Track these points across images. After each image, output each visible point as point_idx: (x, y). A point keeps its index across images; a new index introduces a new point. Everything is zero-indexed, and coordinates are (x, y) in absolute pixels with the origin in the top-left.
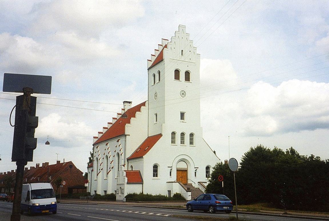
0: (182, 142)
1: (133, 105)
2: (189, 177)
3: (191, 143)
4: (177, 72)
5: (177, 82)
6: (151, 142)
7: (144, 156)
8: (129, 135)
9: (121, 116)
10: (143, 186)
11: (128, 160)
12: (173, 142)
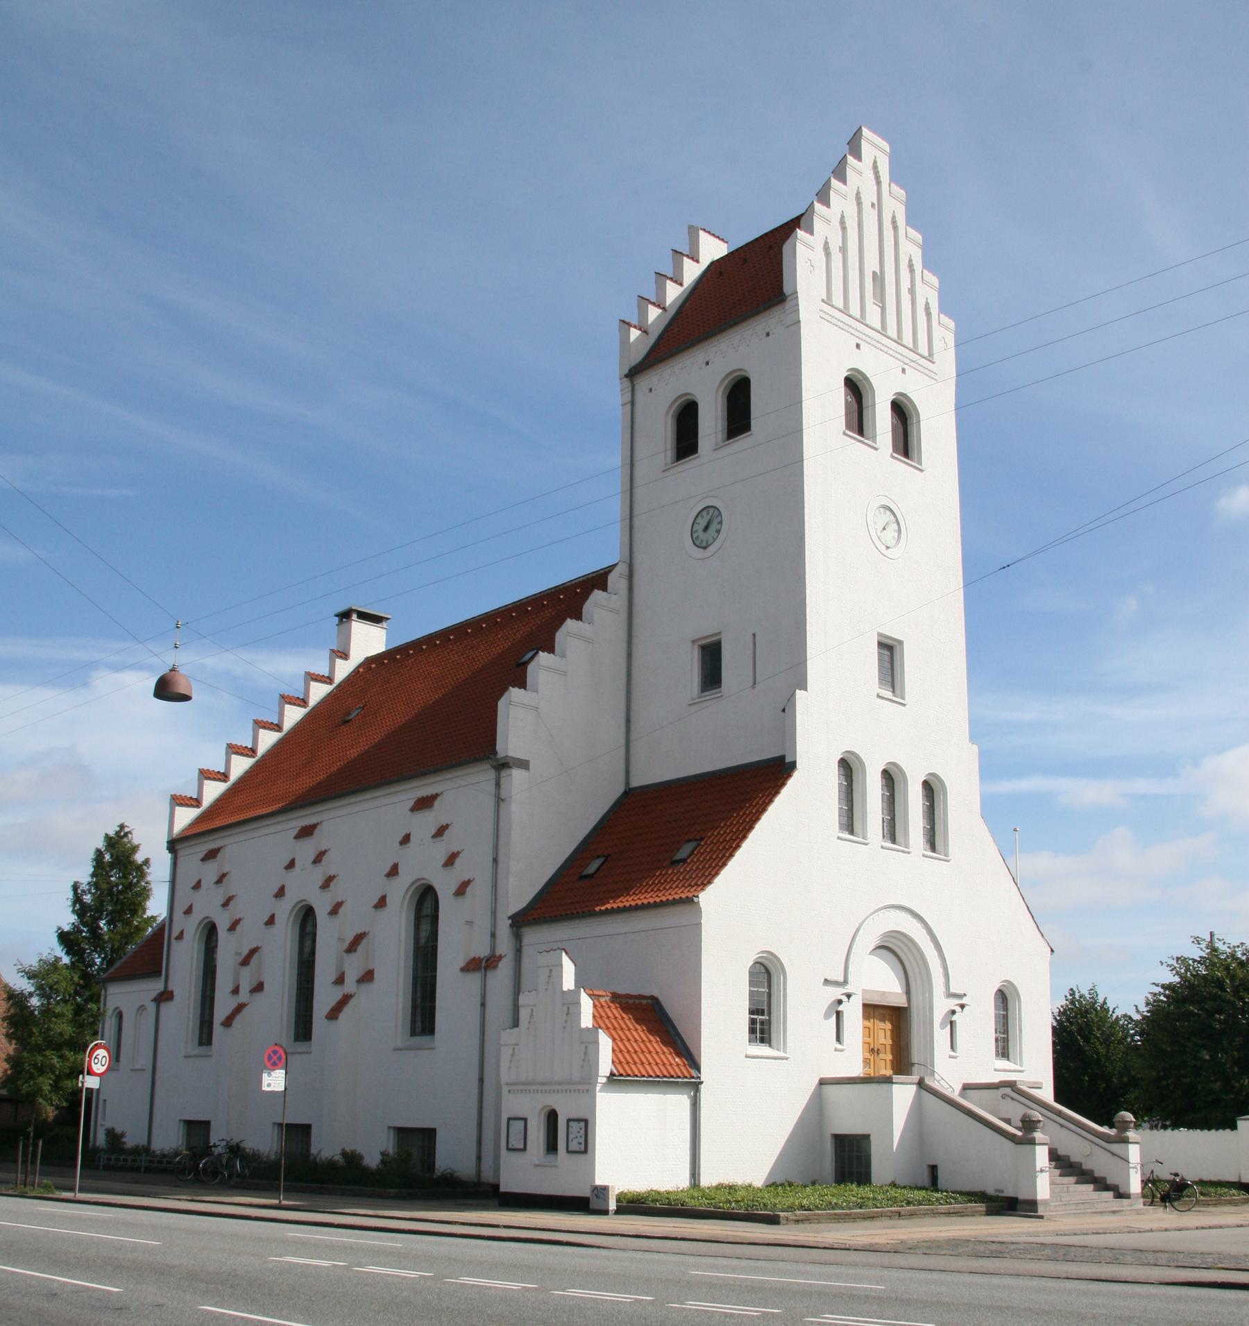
8: (524, 764)
12: (850, 822)
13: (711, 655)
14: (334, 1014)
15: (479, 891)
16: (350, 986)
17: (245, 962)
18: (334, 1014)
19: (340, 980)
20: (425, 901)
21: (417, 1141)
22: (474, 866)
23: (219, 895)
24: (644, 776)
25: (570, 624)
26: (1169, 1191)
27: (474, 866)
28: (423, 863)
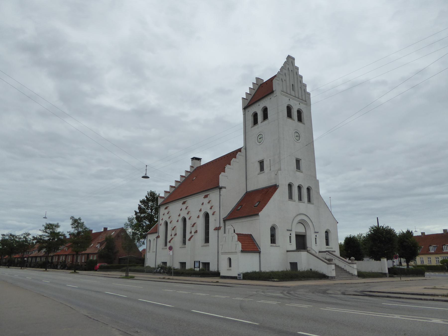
1: (203, 162)
7: (260, 213)
8: (225, 188)
10: (260, 256)
12: (291, 197)
13: (261, 163)
14: (189, 240)
15: (217, 213)
16: (193, 234)
17: (173, 229)
18: (189, 240)
19: (191, 233)
20: (207, 216)
21: (207, 265)
22: (216, 209)
23: (209, 206)
24: (251, 188)
25: (233, 159)
26: (361, 275)
27: (216, 209)
28: (206, 208)
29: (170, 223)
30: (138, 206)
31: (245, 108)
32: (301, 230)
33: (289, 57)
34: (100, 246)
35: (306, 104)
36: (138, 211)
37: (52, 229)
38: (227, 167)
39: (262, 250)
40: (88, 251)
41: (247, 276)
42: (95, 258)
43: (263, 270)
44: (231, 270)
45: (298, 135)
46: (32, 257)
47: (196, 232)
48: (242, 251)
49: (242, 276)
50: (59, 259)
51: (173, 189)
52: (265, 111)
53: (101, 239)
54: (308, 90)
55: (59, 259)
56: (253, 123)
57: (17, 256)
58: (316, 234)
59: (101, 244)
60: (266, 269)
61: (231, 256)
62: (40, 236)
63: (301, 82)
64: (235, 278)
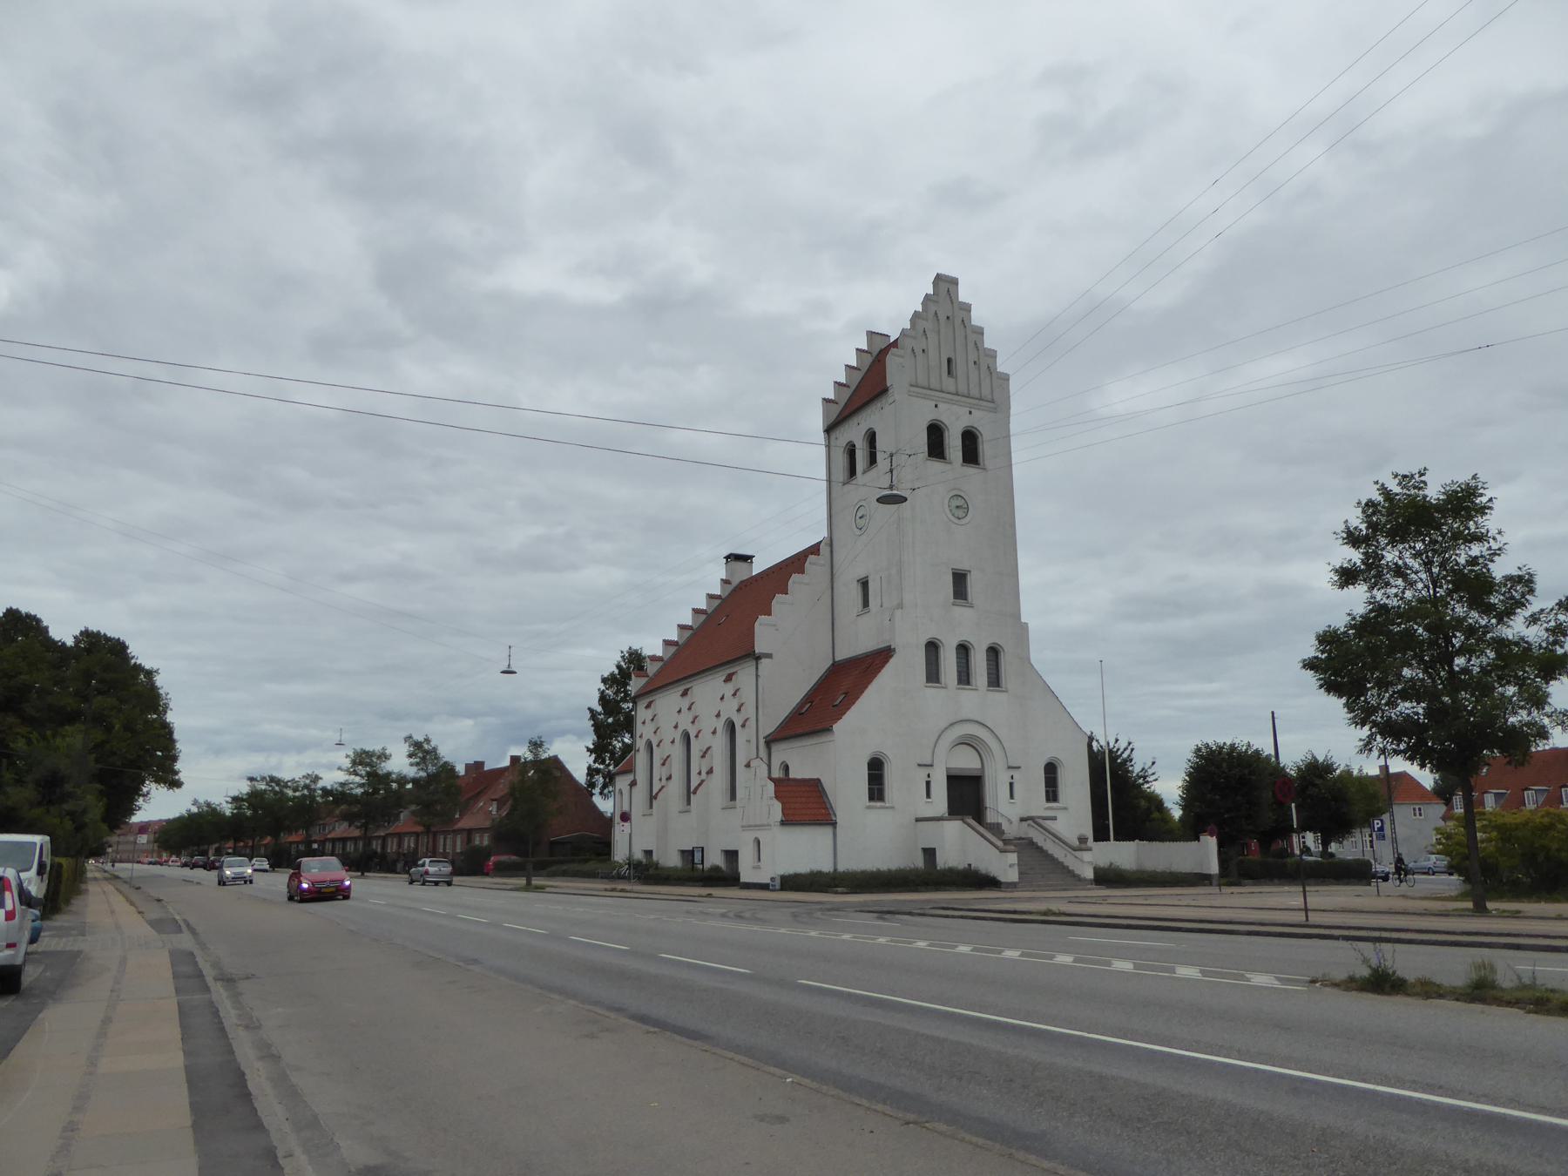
0: (964, 677)
1: (758, 567)
2: (989, 802)
3: (995, 681)
4: (936, 434)
5: (936, 466)
6: (845, 680)
7: (835, 727)
8: (769, 656)
9: (660, 664)
11: (770, 741)
12: (933, 675)
16: (704, 775)
22: (749, 711)
29: (743, 726)
30: (597, 695)
31: (829, 430)
32: (966, 762)
33: (939, 279)
34: (499, 809)
35: (994, 410)
36: (599, 709)
37: (370, 765)
38: (778, 601)
39: (840, 818)
40: (466, 823)
41: (791, 883)
42: (486, 843)
43: (841, 868)
44: (758, 868)
45: (959, 502)
46: (334, 841)
47: (710, 772)
48: (783, 823)
49: (778, 883)
50: (400, 845)
51: (673, 649)
52: (871, 438)
53: (502, 788)
54: (1002, 366)
55: (400, 845)
56: (847, 474)
57: (293, 838)
58: (1012, 772)
59: (501, 802)
60: (847, 864)
61: (761, 835)
62: (342, 785)
63: (978, 346)
64: (763, 887)
